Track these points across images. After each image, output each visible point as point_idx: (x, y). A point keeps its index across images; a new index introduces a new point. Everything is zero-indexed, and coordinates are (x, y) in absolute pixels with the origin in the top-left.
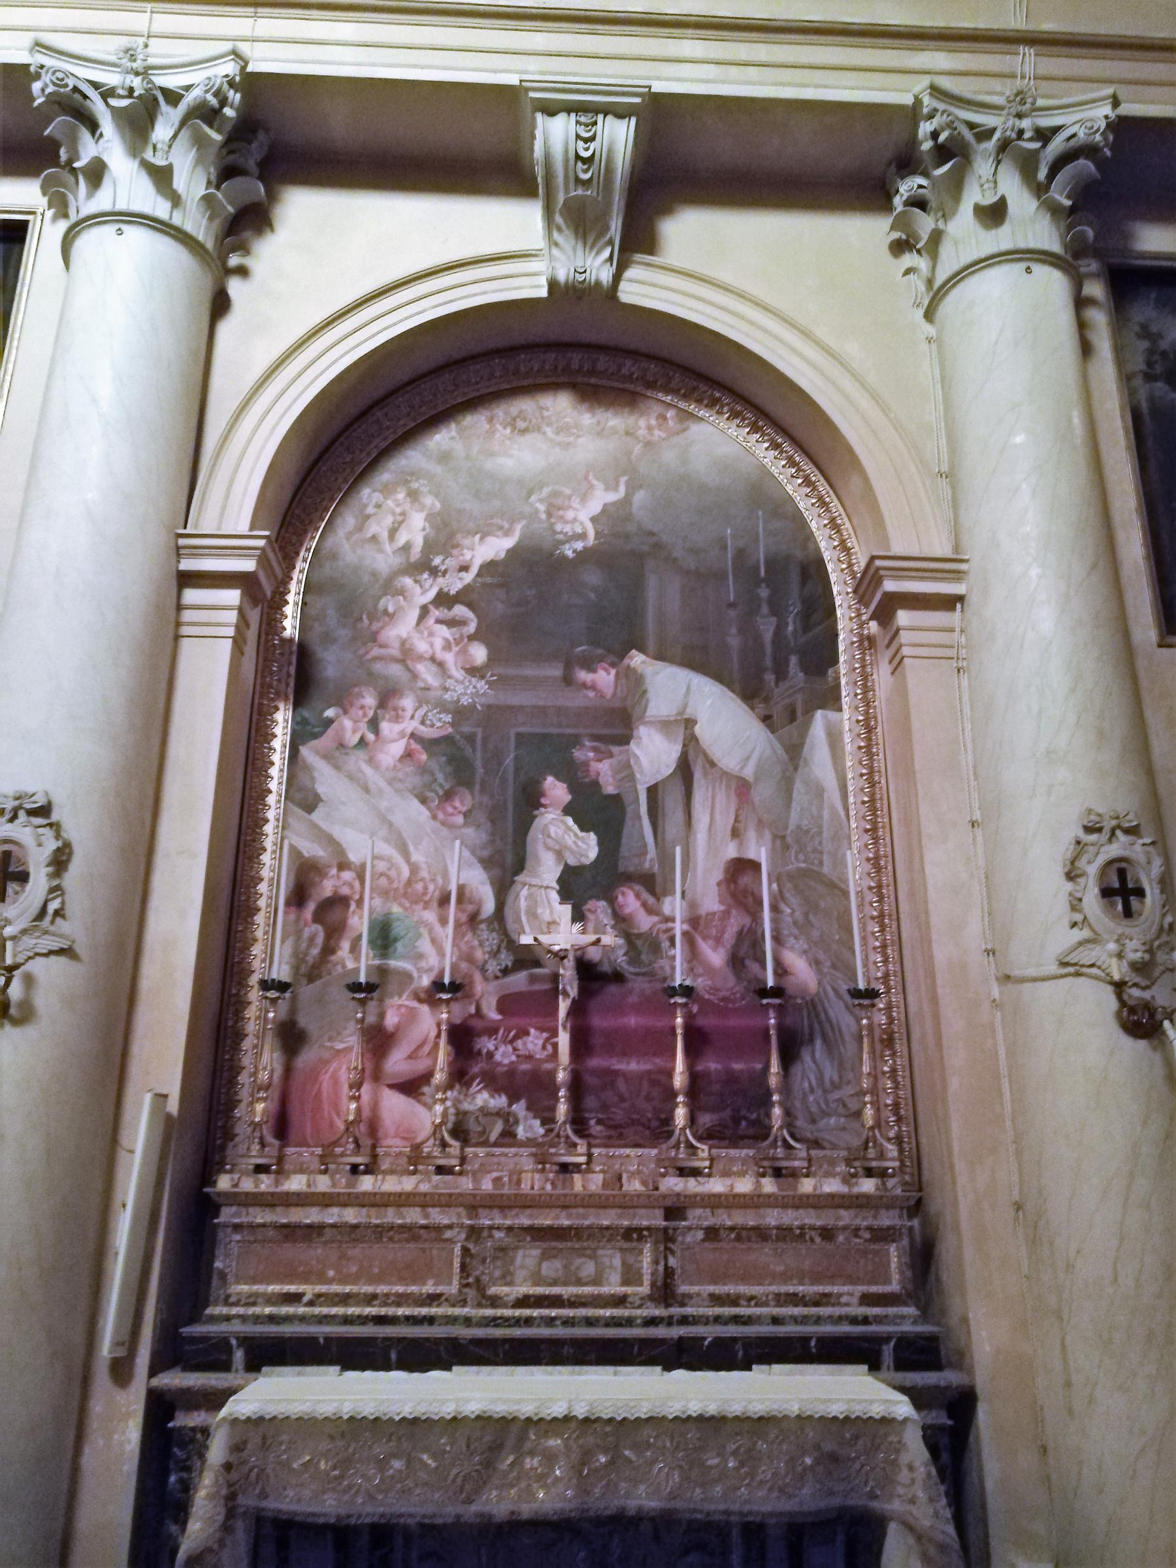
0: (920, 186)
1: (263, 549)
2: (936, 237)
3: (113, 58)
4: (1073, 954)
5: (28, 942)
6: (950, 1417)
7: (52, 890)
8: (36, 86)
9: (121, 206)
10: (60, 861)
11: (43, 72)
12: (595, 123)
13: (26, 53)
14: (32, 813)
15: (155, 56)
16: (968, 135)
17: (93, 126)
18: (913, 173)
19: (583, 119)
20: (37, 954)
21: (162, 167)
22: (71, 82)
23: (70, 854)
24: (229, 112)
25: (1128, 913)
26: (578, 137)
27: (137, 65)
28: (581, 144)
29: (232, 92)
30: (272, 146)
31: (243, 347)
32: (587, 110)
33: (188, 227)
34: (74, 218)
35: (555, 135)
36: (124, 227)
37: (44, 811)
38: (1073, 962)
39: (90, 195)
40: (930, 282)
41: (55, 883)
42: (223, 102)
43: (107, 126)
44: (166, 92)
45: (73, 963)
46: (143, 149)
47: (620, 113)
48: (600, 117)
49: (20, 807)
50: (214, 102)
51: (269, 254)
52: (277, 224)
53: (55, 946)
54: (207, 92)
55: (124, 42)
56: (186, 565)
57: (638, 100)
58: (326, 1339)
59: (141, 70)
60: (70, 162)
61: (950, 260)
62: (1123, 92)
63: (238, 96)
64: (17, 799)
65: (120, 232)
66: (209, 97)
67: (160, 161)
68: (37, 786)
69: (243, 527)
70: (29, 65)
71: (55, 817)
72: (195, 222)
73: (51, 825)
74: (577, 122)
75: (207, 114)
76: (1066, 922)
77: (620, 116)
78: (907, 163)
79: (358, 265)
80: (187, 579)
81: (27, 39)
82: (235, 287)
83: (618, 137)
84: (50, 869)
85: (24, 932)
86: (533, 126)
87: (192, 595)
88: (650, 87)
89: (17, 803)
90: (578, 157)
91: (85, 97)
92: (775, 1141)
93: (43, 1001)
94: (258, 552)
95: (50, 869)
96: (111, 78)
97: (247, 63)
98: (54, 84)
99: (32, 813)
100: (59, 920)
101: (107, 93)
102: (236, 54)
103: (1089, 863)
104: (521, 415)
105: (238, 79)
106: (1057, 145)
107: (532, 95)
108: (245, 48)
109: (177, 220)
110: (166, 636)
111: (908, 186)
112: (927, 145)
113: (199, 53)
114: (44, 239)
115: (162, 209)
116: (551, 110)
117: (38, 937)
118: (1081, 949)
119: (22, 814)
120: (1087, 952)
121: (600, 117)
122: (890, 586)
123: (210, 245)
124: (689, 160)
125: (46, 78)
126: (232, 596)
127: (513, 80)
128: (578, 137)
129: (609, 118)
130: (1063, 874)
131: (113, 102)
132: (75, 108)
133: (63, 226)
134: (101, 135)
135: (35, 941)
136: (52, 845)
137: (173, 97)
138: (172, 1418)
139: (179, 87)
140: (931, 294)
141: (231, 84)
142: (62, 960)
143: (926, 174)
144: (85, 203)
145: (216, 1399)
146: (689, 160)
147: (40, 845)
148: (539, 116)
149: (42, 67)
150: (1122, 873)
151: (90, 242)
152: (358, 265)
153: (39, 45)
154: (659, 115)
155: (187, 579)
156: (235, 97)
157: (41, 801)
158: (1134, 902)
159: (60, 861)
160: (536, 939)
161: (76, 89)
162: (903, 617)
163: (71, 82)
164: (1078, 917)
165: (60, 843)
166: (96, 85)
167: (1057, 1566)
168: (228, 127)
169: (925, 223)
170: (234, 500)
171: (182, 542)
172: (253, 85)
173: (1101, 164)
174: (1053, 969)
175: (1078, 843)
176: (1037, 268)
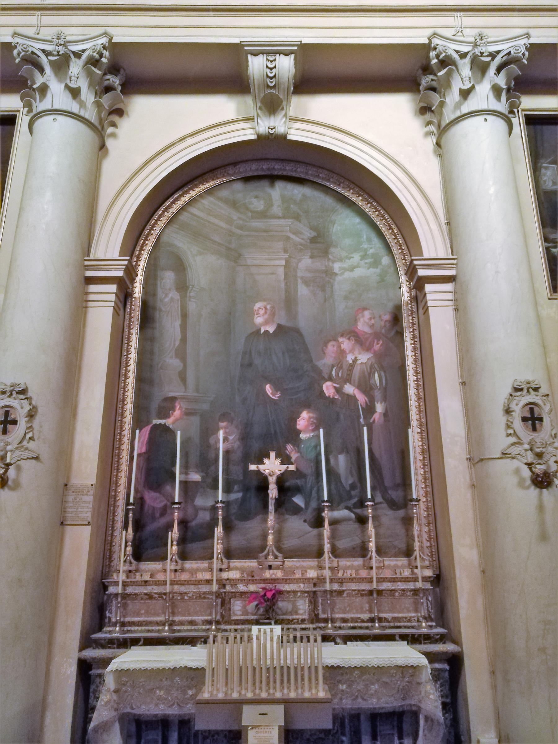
0: (432, 80)
1: (126, 266)
2: (442, 104)
3: (49, 38)
4: (508, 450)
5: (18, 453)
7: (28, 428)
8: (15, 52)
9: (56, 107)
10: (31, 415)
11: (18, 45)
12: (275, 60)
13: (10, 37)
14: (18, 393)
15: (69, 35)
16: (455, 56)
17: (42, 70)
18: (431, 74)
20: (22, 459)
21: (73, 88)
23: (36, 412)
24: (104, 60)
25: (534, 429)
27: (61, 41)
28: (268, 70)
29: (105, 51)
30: (129, 74)
33: (87, 116)
34: (34, 112)
35: (256, 66)
37: (23, 392)
38: (509, 453)
39: (41, 100)
40: (439, 126)
41: (29, 425)
42: (101, 55)
43: (48, 70)
44: (73, 53)
45: (39, 464)
46: (66, 79)
47: (287, 54)
48: (278, 55)
49: (13, 390)
50: (97, 56)
51: (126, 127)
52: (130, 113)
53: (30, 456)
54: (93, 52)
55: (55, 30)
57: (296, 48)
58: (123, 639)
59: (63, 43)
60: (32, 86)
61: (449, 115)
62: (531, 31)
63: (107, 52)
64: (11, 386)
66: (95, 54)
67: (73, 85)
68: (21, 380)
69: (116, 256)
70: (11, 43)
71: (30, 394)
72: (90, 114)
73: (27, 398)
74: (267, 59)
75: (94, 62)
76: (505, 434)
77: (286, 55)
78: (427, 69)
79: (172, 127)
80: (90, 281)
81: (11, 31)
82: (110, 143)
83: (286, 65)
84: (27, 419)
85: (17, 448)
86: (247, 61)
87: (93, 288)
88: (301, 42)
89: (12, 388)
90: (267, 76)
91: (38, 56)
92: (269, 552)
93: (24, 479)
94: (124, 267)
95: (27, 419)
96: (48, 47)
97: (112, 38)
98: (23, 51)
99: (18, 393)
100: (31, 441)
101: (47, 53)
102: (105, 34)
103: (517, 405)
105: (107, 45)
106: (498, 60)
107: (246, 48)
108: (111, 31)
109: (82, 113)
110: (79, 308)
111: (425, 81)
112: (435, 61)
113: (86, 34)
114: (23, 122)
115: (75, 107)
117: (23, 451)
118: (513, 447)
119: (14, 393)
120: (516, 448)
122: (421, 273)
123: (96, 123)
124: (327, 72)
125: (19, 48)
126: (113, 288)
127: (236, 40)
129: (282, 55)
130: (503, 410)
131: (51, 58)
132: (32, 61)
135: (21, 453)
136: (27, 408)
137: (78, 55)
139: (79, 51)
140: (440, 132)
141: (104, 48)
142: (34, 461)
143: (435, 75)
144: (41, 106)
146: (327, 72)
147: (22, 408)
148: (249, 56)
149: (17, 43)
150: (532, 410)
151: (40, 123)
152: (172, 127)
153: (15, 34)
154: (304, 52)
155: (90, 281)
156: (106, 53)
157: (23, 387)
159: (31, 415)
160: (258, 467)
161: (33, 53)
162: (428, 288)
163: (30, 49)
164: (510, 431)
165: (31, 407)
166: (44, 51)
167: (499, 741)
168: (104, 67)
169: (436, 98)
170: (109, 244)
171: (87, 263)
172: (115, 47)
173: (522, 67)
174: (498, 456)
175: (511, 395)
176: (489, 117)
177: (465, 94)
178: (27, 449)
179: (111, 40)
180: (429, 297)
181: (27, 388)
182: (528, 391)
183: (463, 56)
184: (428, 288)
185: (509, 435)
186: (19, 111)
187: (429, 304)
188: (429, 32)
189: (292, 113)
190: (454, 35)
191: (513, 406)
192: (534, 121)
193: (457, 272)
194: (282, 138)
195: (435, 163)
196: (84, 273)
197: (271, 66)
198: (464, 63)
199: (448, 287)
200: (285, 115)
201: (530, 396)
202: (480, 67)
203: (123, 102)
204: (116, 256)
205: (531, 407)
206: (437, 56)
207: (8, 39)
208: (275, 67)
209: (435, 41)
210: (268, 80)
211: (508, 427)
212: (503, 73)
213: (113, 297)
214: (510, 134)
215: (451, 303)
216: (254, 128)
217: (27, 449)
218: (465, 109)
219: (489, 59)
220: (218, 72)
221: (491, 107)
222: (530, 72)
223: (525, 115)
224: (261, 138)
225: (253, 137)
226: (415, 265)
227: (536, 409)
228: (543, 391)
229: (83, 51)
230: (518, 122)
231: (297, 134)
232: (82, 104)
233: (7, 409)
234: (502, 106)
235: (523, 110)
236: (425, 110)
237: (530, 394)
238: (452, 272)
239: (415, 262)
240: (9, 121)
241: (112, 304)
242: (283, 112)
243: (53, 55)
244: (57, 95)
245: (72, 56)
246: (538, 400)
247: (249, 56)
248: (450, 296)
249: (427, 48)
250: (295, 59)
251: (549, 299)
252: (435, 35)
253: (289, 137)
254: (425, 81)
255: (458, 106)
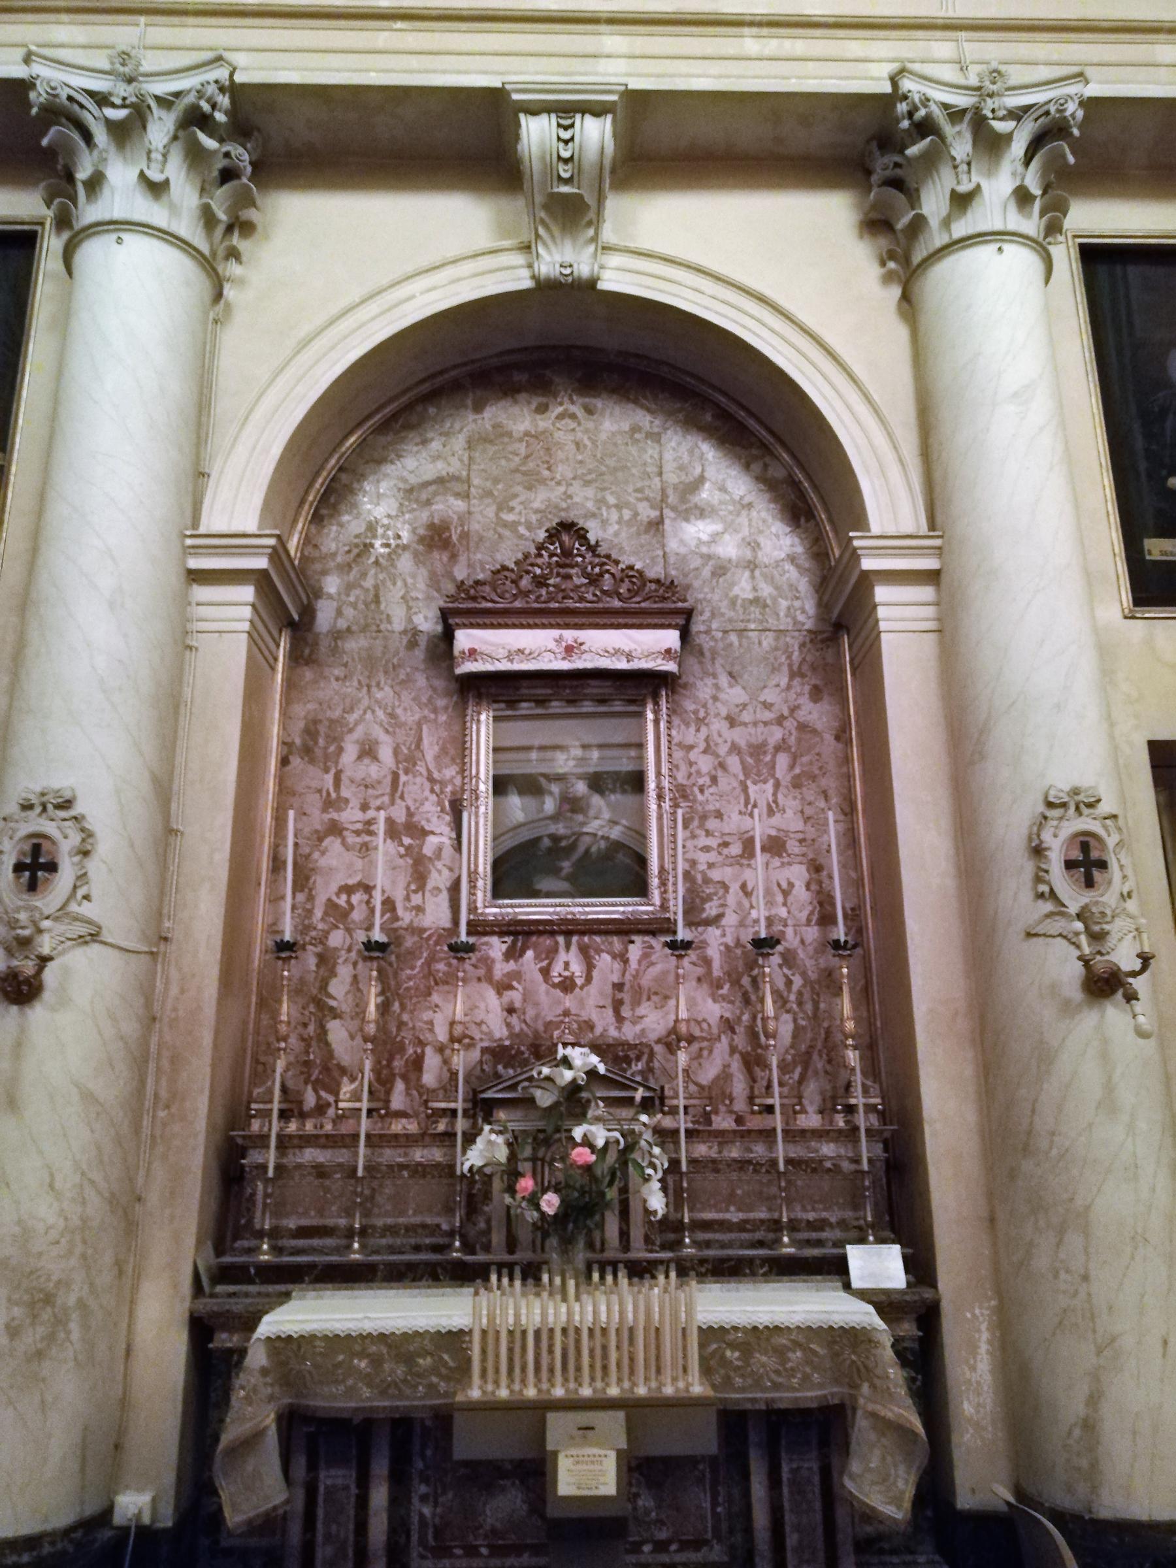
1: (273, 547)
6: (919, 1329)
12: (572, 126)
19: (562, 122)
22: (64, 93)
24: (220, 117)
25: (1089, 883)
26: (559, 139)
28: (561, 145)
30: (272, 145)
31: (238, 348)
32: (567, 111)
35: (536, 133)
36: (124, 236)
37: (66, 804)
44: (158, 98)
47: (597, 110)
56: (194, 563)
57: (614, 98)
65: (119, 241)
71: (78, 809)
72: (187, 227)
74: (559, 125)
83: (595, 133)
86: (518, 125)
87: (203, 593)
94: (269, 551)
97: (235, 69)
101: (102, 99)
104: (501, 433)
107: (515, 97)
111: (882, 164)
112: (905, 124)
113: (175, 56)
114: (51, 245)
116: (534, 110)
121: (578, 116)
122: (867, 564)
124: (675, 143)
128: (559, 139)
131: (111, 113)
132: (60, 112)
133: (66, 235)
134: (95, 145)
136: (75, 838)
138: (211, 1340)
145: (251, 1322)
146: (675, 143)
148: (522, 116)
150: (1085, 847)
151: (93, 252)
154: (637, 109)
156: (224, 101)
158: (1076, 854)
163: (64, 93)
164: (1044, 888)
170: (239, 502)
177: (962, 201)
178: (76, 919)
179: (231, 75)
180: (881, 612)
181: (75, 798)
182: (1077, 808)
183: (956, 115)
184: (882, 593)
185: (1041, 896)
186: (42, 224)
187: (883, 626)
188: (893, 67)
189: (608, 234)
190: (939, 75)
191: (1047, 836)
192: (1097, 258)
193: (943, 565)
194: (591, 284)
195: (901, 332)
196: (184, 562)
197: (566, 135)
198: (959, 133)
199: (926, 593)
200: (594, 239)
201: (1083, 818)
202: (990, 144)
203: (253, 204)
204: (251, 526)
205: (1085, 842)
206: (910, 115)
207: (18, 71)
208: (572, 139)
209: (907, 85)
210: (561, 167)
211: (1038, 880)
212: (1035, 164)
213: (247, 612)
214: (1047, 280)
215: (931, 625)
216: (530, 266)
217: (76, 919)
218: (960, 229)
219: (1012, 124)
220: (456, 142)
221: (1011, 226)
222: (1091, 147)
223: (1081, 246)
224: (547, 289)
225: (527, 284)
226: (855, 549)
227: (1093, 843)
228: (1105, 808)
229: (177, 95)
230: (1065, 257)
231: (618, 278)
232: (174, 209)
233: (35, 841)
234: (1031, 225)
235: (1075, 236)
236: (876, 224)
237: (1080, 814)
238: (930, 564)
239: (856, 543)
240: (19, 243)
241: (246, 626)
242: (591, 232)
243: (113, 106)
244: (121, 193)
245: (153, 104)
246: (1096, 827)
247: (522, 116)
248: (930, 611)
249: (884, 103)
250: (614, 121)
251: (1126, 617)
252: (902, 71)
253: (603, 285)
254: (882, 164)
255: (946, 223)
